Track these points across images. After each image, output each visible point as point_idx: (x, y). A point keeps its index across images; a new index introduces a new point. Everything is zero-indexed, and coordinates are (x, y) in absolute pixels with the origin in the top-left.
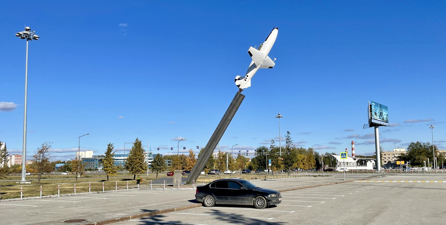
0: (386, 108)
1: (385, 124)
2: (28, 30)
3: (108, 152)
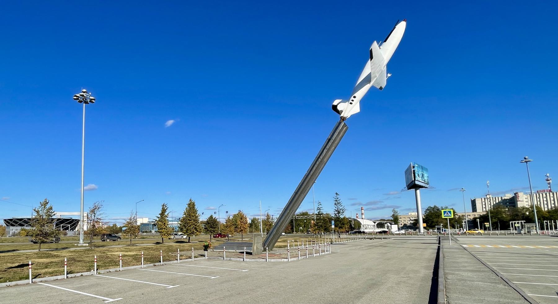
2: (85, 92)
3: (163, 213)
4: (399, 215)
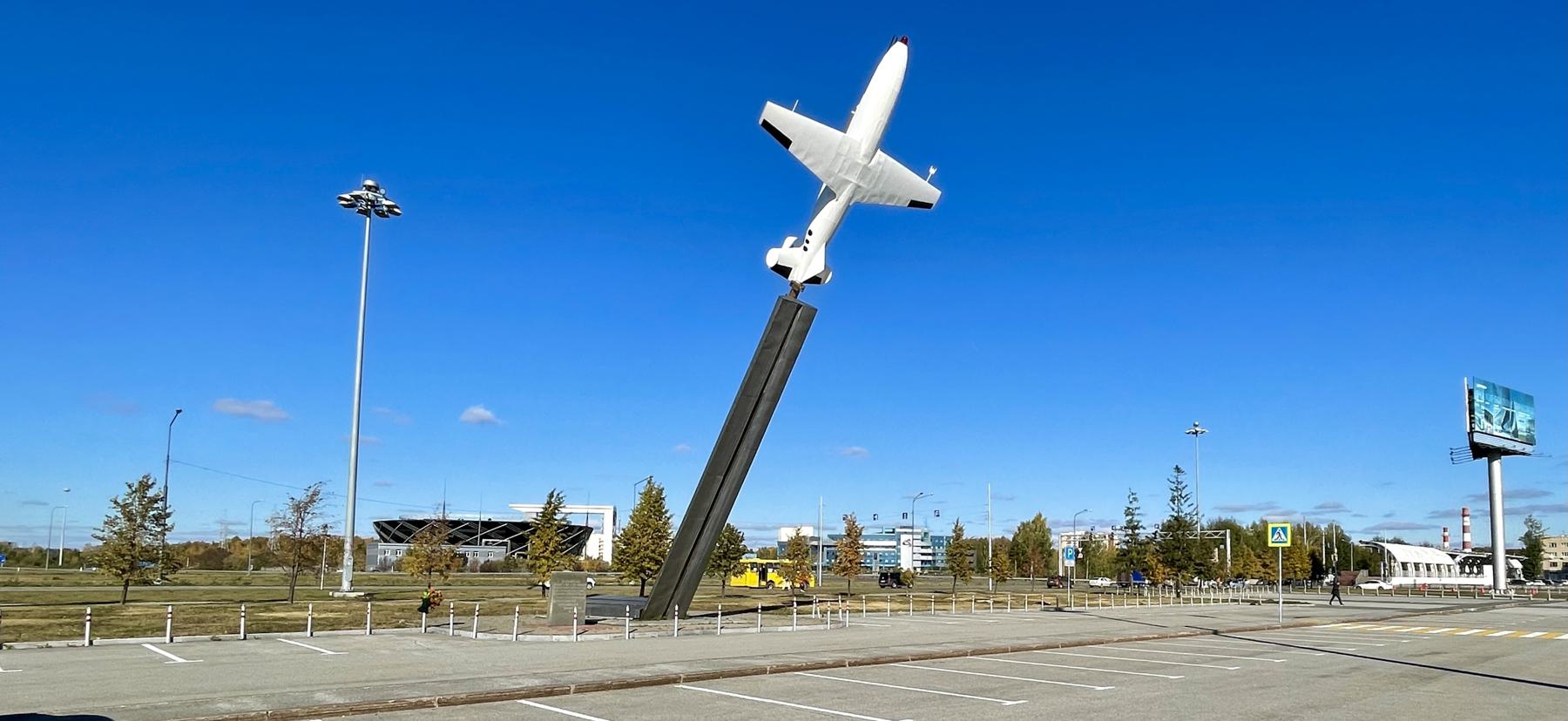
0: (1528, 400)
1: (1528, 449)
2: (369, 188)
4: (1546, 534)
